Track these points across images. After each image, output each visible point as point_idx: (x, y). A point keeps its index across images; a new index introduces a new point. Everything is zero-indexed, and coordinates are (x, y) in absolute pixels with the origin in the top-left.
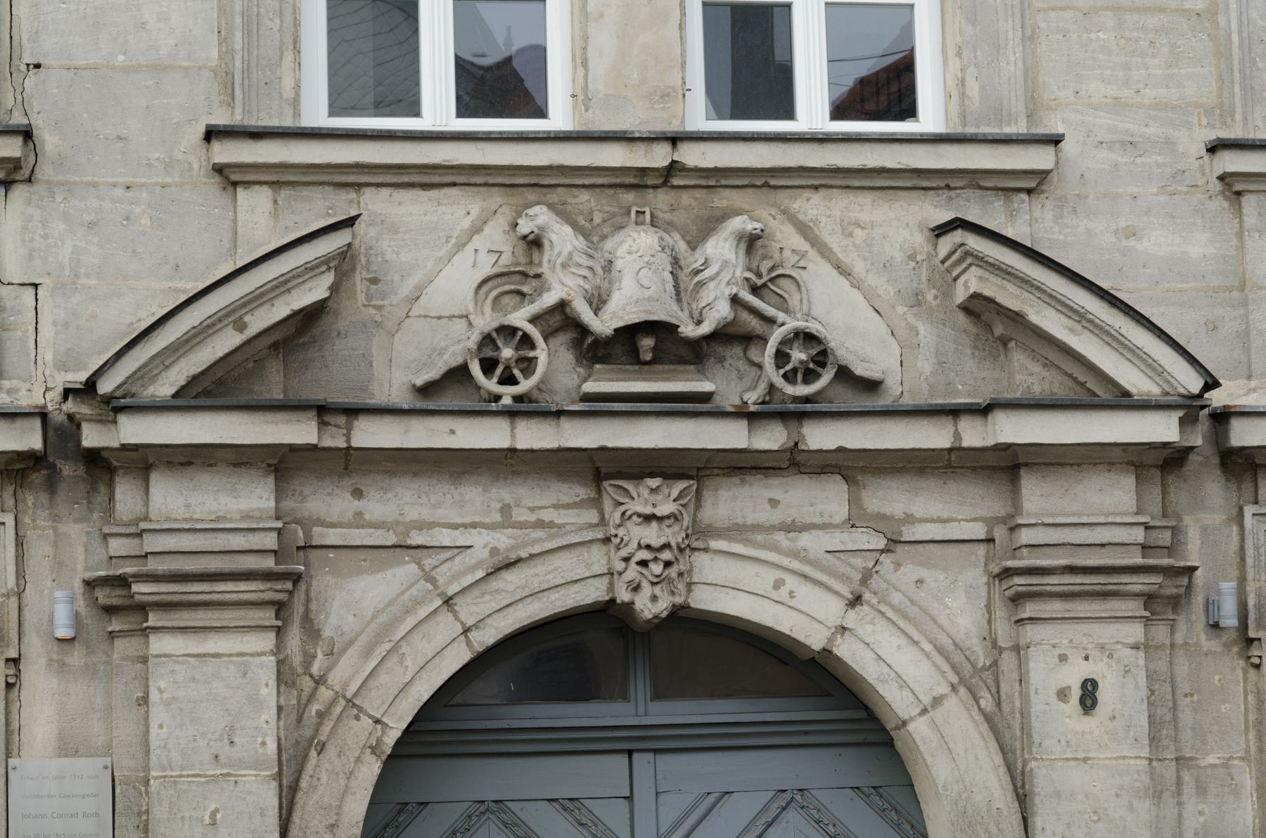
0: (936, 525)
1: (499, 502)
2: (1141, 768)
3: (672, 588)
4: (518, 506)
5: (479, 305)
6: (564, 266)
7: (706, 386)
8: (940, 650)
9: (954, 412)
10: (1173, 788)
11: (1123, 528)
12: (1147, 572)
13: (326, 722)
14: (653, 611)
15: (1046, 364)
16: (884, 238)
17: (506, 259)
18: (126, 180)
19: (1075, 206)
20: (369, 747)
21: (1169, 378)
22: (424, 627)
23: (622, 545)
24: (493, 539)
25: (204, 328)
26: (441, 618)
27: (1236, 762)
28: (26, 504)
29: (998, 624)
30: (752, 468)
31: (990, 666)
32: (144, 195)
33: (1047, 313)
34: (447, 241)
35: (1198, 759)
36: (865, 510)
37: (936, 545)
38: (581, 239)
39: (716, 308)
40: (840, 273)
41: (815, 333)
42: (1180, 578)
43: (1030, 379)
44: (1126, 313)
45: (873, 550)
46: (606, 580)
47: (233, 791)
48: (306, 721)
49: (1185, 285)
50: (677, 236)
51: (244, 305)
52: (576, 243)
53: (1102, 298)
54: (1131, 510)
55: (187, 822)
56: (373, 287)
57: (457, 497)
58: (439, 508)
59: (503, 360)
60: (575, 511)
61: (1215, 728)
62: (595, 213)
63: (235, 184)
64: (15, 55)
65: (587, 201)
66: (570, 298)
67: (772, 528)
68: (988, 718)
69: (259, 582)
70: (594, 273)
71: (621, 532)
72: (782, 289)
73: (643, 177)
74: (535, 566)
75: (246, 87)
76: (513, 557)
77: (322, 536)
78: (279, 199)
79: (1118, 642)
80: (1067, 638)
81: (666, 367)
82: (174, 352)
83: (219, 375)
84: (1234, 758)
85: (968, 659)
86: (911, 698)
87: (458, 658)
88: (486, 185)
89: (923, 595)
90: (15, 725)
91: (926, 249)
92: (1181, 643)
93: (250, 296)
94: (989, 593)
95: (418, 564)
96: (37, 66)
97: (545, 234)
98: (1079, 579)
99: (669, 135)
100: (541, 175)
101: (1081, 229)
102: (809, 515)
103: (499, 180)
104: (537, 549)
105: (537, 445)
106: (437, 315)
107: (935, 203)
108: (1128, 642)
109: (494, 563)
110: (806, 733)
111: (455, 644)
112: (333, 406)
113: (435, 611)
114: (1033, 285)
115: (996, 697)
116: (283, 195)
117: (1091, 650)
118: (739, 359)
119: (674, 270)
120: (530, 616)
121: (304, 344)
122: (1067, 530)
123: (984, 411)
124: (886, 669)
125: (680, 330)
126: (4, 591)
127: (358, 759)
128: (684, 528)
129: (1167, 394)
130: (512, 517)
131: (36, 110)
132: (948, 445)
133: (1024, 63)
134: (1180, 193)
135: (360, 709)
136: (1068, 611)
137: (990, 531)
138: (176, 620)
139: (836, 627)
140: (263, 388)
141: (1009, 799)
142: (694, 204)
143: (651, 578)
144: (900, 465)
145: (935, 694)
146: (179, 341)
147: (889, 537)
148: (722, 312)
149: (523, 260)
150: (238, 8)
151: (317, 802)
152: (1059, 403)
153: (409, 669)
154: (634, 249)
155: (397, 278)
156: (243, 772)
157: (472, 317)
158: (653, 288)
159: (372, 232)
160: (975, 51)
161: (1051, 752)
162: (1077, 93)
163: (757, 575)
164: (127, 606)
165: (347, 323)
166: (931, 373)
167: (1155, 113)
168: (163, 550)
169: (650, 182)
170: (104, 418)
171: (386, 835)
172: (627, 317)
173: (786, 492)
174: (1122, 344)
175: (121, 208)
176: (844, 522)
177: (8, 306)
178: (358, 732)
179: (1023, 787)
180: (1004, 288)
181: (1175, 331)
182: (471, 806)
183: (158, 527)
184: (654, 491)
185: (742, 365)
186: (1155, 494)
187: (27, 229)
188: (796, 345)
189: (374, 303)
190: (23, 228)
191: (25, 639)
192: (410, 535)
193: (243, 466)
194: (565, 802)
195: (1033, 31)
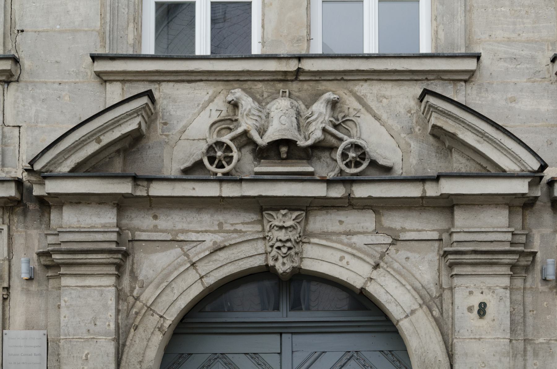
0: (416, 233)
2: (506, 343)
3: (293, 260)
4: (226, 223)
5: (211, 134)
6: (247, 115)
7: (310, 169)
8: (415, 289)
9: (423, 180)
10: (522, 353)
11: (501, 234)
12: (511, 254)
13: (138, 317)
14: (283, 269)
15: (468, 159)
16: (396, 103)
17: (224, 114)
18: (59, 80)
19: (487, 88)
20: (158, 328)
21: (524, 163)
22: (183, 276)
23: (270, 240)
24: (215, 238)
25: (81, 141)
26: (190, 272)
27: (553, 342)
28: (14, 221)
29: (443, 277)
30: (331, 207)
31: (439, 296)
32: (67, 87)
34: (198, 106)
35: (535, 340)
36: (383, 226)
37: (415, 242)
38: (256, 103)
39: (315, 134)
40: (376, 119)
41: (360, 145)
43: (461, 166)
44: (504, 133)
45: (386, 244)
46: (264, 256)
47: (95, 345)
48: (130, 316)
49: (538, 124)
50: (300, 103)
51: (100, 131)
52: (253, 105)
53: (493, 126)
54: (506, 226)
55: (75, 358)
56: (165, 126)
57: (199, 219)
58: (191, 224)
59: (217, 157)
60: (252, 225)
61: (544, 326)
62: (264, 93)
63: (106, 81)
64: (13, 26)
65: (261, 88)
66: (249, 129)
67: (340, 234)
68: (436, 320)
69: (107, 254)
70: (261, 119)
71: (270, 234)
72: (347, 126)
73: (286, 76)
74: (232, 250)
75: (111, 39)
76: (222, 245)
77: (139, 236)
78: (124, 88)
79: (497, 286)
80: (473, 284)
81: (293, 161)
82: (68, 152)
83: (93, 164)
84: (551, 340)
85: (428, 293)
86: (401, 310)
87: (197, 290)
88: (215, 80)
89: (409, 264)
90: (7, 316)
91: (416, 108)
92: (529, 287)
93: (102, 127)
94: (439, 264)
95: (181, 248)
96: (22, 31)
97: (240, 101)
98: (479, 257)
99: (297, 56)
100: (240, 75)
101: (490, 98)
102: (357, 228)
103: (221, 78)
104: (233, 242)
105: (231, 195)
106: (193, 139)
107: (421, 87)
108: (502, 286)
109: (213, 248)
110: (359, 326)
111: (197, 284)
112: (141, 177)
113: (187, 269)
114: (460, 121)
115: (441, 310)
116: (126, 86)
117: (484, 289)
118: (328, 158)
119: (298, 117)
120: (230, 271)
121: (134, 152)
122: (475, 235)
123: (437, 179)
124: (390, 297)
125: (297, 143)
126: (1, 258)
127: (152, 333)
128: (298, 232)
129: (523, 171)
130: (223, 228)
131: (21, 50)
132: (420, 195)
133: (465, 21)
134: (537, 81)
135: (154, 311)
137: (440, 235)
138: (72, 271)
139: (368, 278)
140: (112, 170)
141: (444, 356)
142: (309, 88)
143: (282, 255)
144: (400, 205)
145: (412, 309)
146: (70, 147)
148: (317, 136)
149: (231, 114)
150: (108, 3)
151: (134, 352)
152: (471, 175)
153: (176, 294)
154: (279, 107)
155: (175, 122)
156: (100, 337)
157: (208, 139)
158: (287, 124)
159: (165, 102)
160: (443, 18)
161: (464, 335)
162: (490, 36)
163: (332, 254)
164: (53, 265)
165: (153, 142)
166: (416, 164)
167: (527, 45)
168: (67, 241)
169: (289, 78)
170: (41, 182)
171: (174, 367)
172: (273, 138)
173: (347, 217)
174: (502, 147)
175: (57, 93)
176: (373, 231)
177: (7, 136)
178: (152, 321)
179: (452, 351)
180: (447, 122)
181: (532, 145)
182: (210, 356)
183: (64, 230)
184: (284, 215)
185: (329, 160)
186: (518, 220)
187: (16, 102)
188: (351, 150)
189: (165, 133)
190: (14, 102)
191: (12, 279)
192: (178, 236)
193: (103, 204)
194: (251, 355)
195: (470, 8)
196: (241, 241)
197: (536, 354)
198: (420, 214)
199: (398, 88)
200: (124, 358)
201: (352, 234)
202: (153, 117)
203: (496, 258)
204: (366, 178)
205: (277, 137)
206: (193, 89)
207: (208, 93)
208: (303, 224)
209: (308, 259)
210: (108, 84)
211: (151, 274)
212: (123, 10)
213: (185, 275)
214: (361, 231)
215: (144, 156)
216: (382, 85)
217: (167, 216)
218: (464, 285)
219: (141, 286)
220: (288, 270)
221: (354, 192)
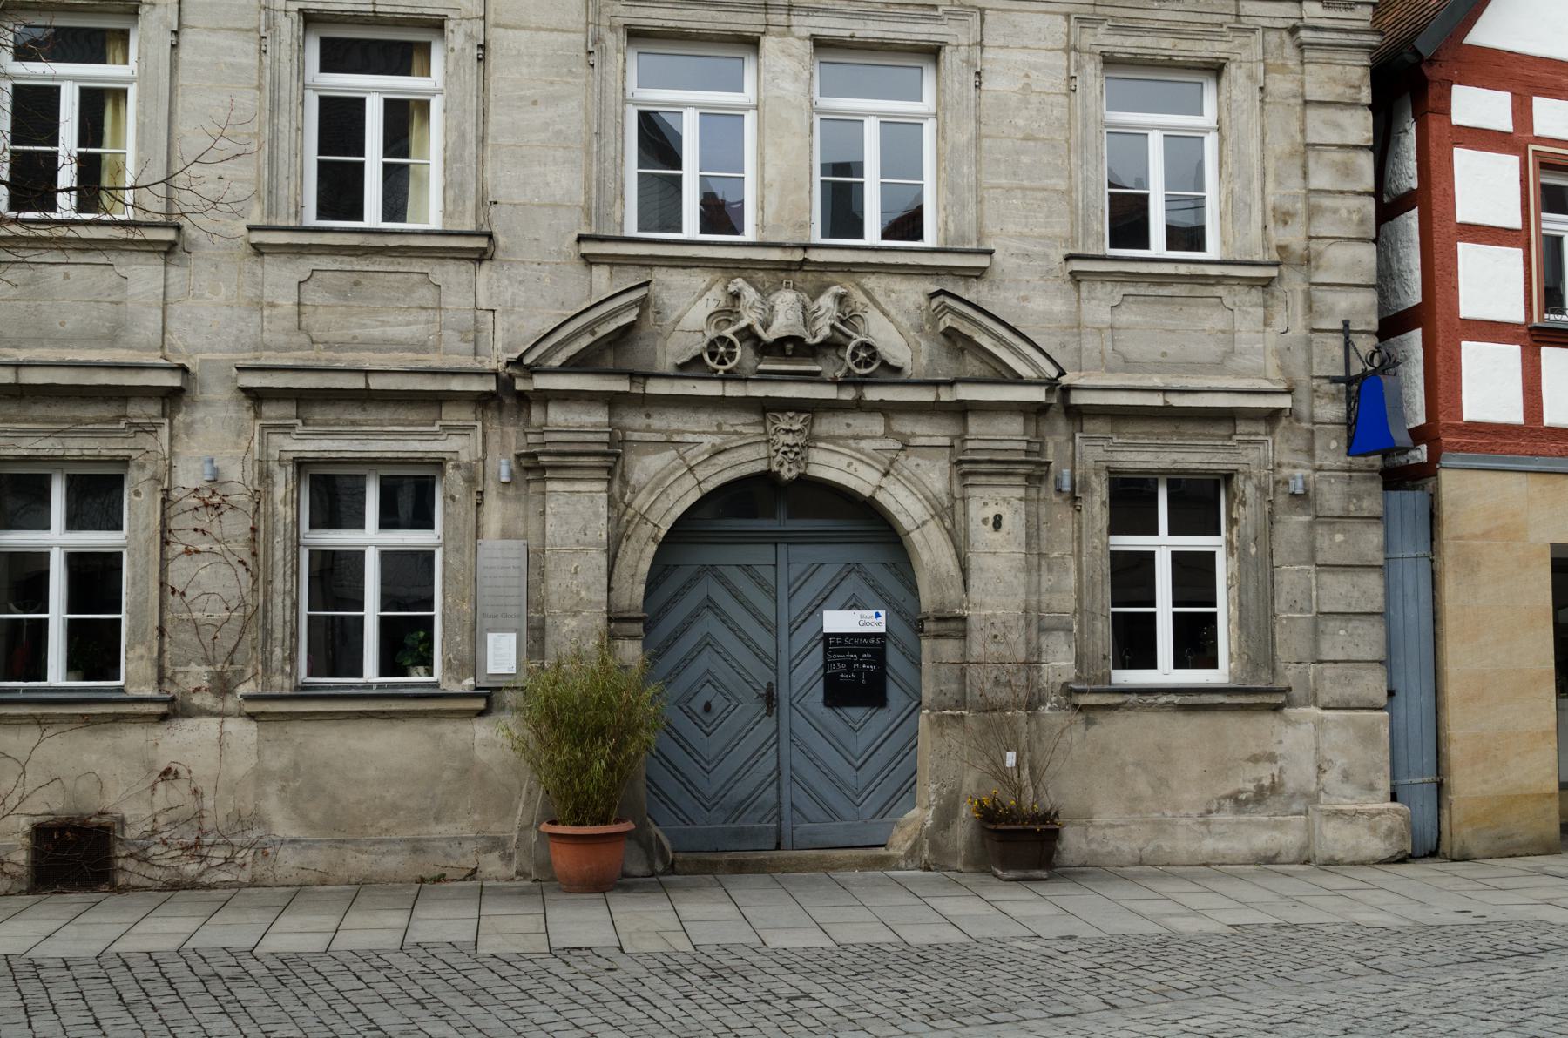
7: (818, 368)
8: (927, 498)
9: (937, 384)
18: (539, 260)
63: (591, 264)
67: (848, 438)
68: (948, 532)
104: (734, 445)
123: (951, 384)
159: (658, 289)
185: (835, 358)
186: (1033, 426)
197: (1050, 570)
200: (616, 571)
204: (879, 380)
205: (783, 334)
210: (594, 268)
211: (643, 478)
213: (682, 481)
217: (661, 414)
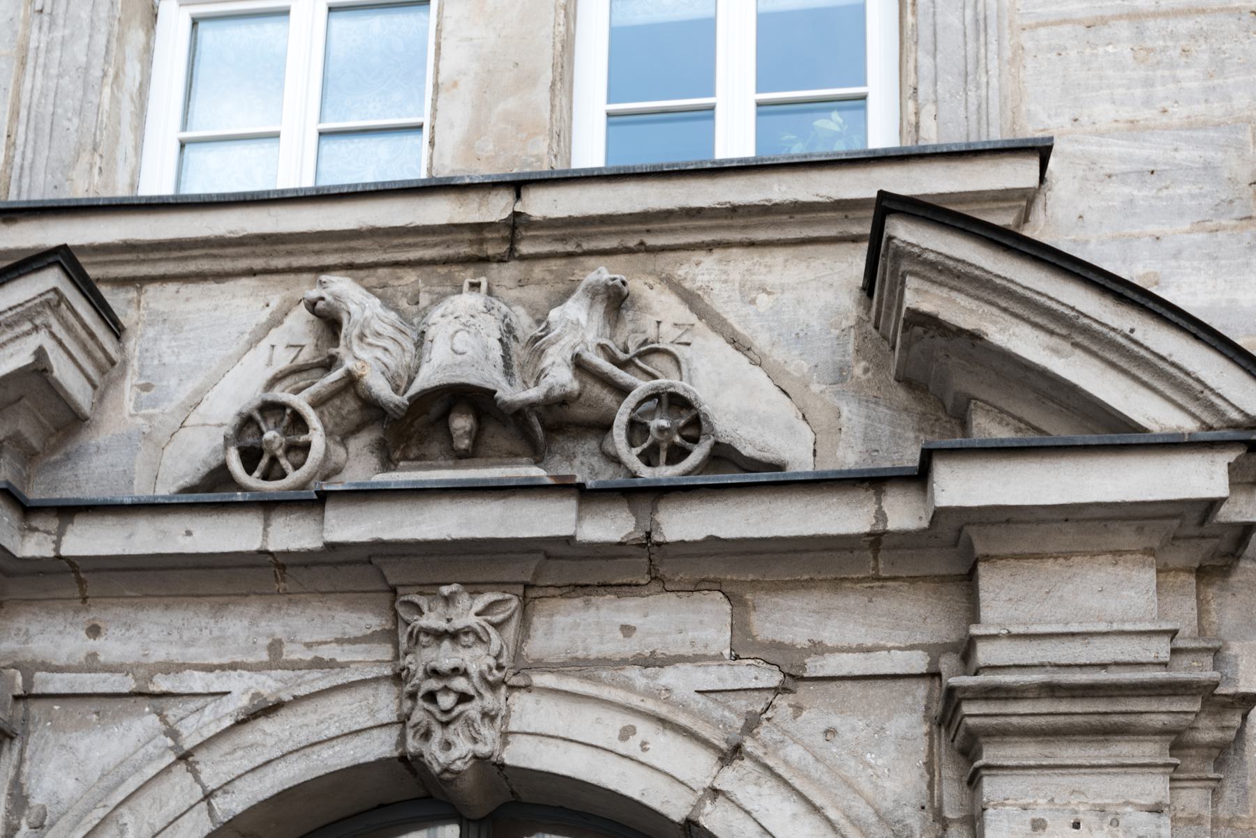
0: (856, 655)
1: (268, 637)
3: (475, 735)
4: (292, 641)
22: (154, 790)
30: (599, 586)
33: (1017, 330)
36: (753, 637)
37: (855, 683)
40: (737, 349)
41: (682, 393)
42: (1228, 716)
56: (145, 394)
58: (193, 646)
60: (364, 646)
67: (624, 662)
74: (305, 714)
76: (272, 700)
77: (46, 682)
79: (1127, 803)
80: (1045, 797)
94: (931, 747)
105: (294, 546)
108: (1143, 802)
111: (193, 813)
113: (168, 769)
117: (1084, 813)
120: (294, 777)
121: (56, 462)
122: (1047, 645)
125: (496, 395)
130: (281, 654)
132: (867, 529)
134: (1224, 228)
136: (1046, 757)
137: (934, 661)
139: (705, 790)
142: (548, 277)
144: (806, 577)
147: (786, 670)
162: (1076, 120)
167: (1188, 133)
188: (658, 414)
189: (144, 411)
192: (154, 680)
196: (328, 686)
198: (870, 601)
199: (803, 265)
201: (658, 663)
202: (114, 372)
203: (1123, 709)
206: (230, 296)
207: (268, 305)
208: (511, 630)
209: (525, 737)
212: (66, 124)
213: (161, 789)
214: (686, 655)
215: (81, 472)
216: (756, 259)
218: (1016, 800)
219: (37, 824)
220: (459, 763)
221: (662, 526)
